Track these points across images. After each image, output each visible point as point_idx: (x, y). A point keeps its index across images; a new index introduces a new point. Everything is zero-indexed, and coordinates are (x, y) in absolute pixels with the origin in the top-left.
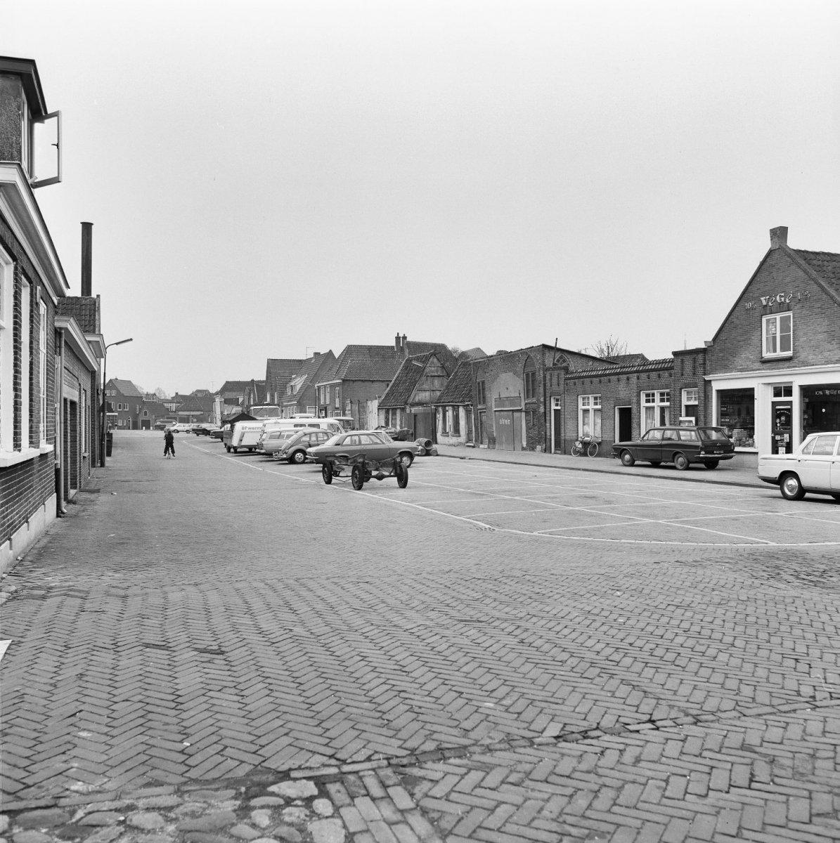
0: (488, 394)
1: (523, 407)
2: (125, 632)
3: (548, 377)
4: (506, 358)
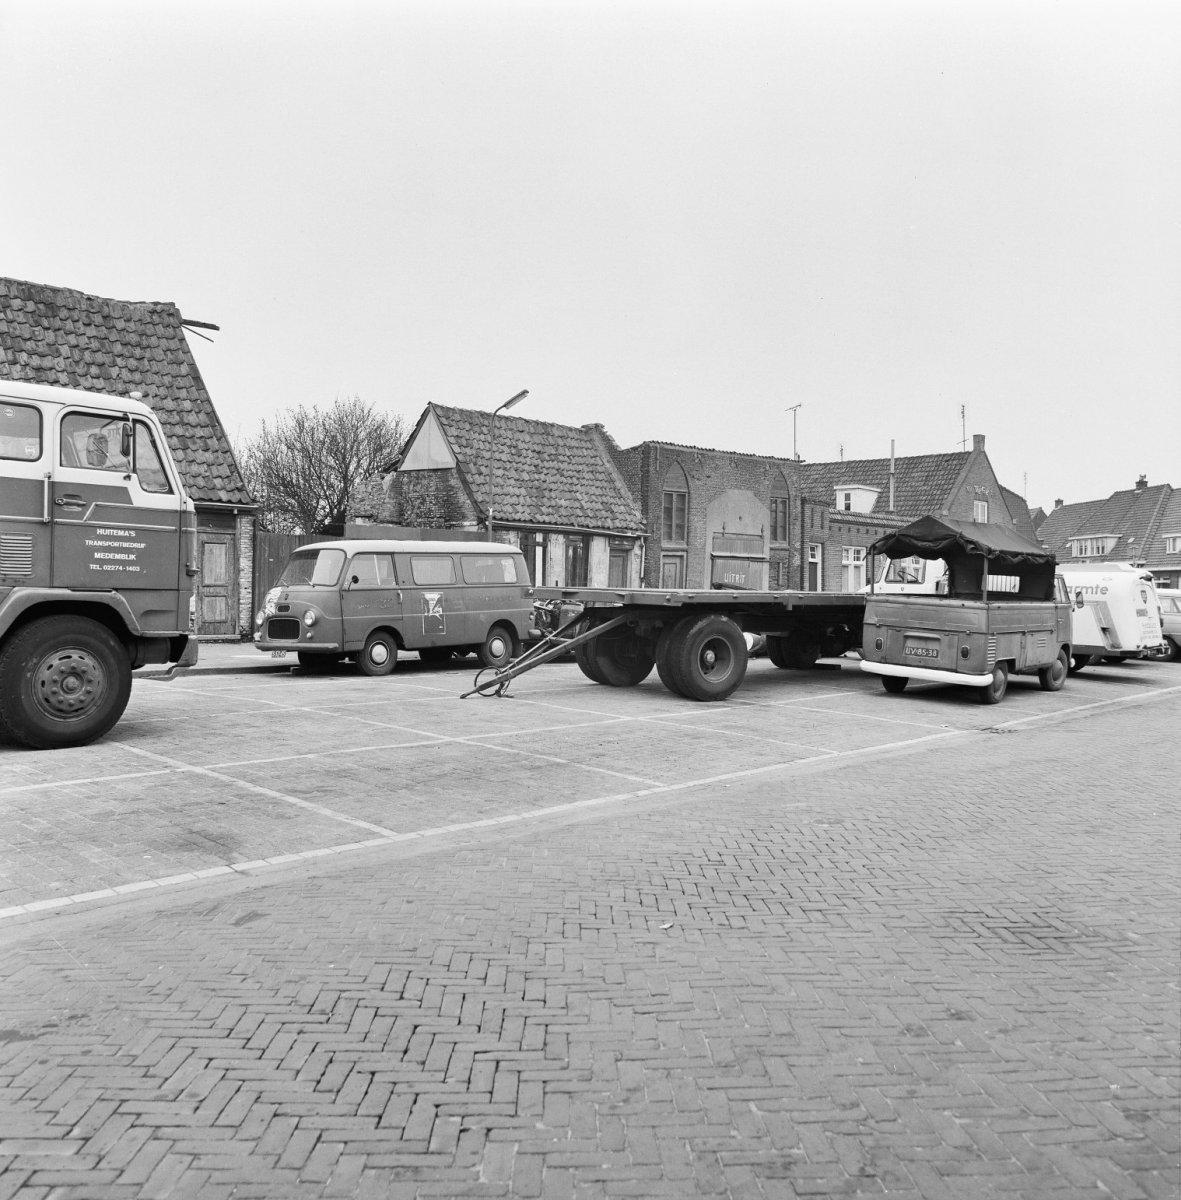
0: (696, 522)
1: (766, 555)
2: (395, 954)
3: (808, 513)
4: (747, 467)
